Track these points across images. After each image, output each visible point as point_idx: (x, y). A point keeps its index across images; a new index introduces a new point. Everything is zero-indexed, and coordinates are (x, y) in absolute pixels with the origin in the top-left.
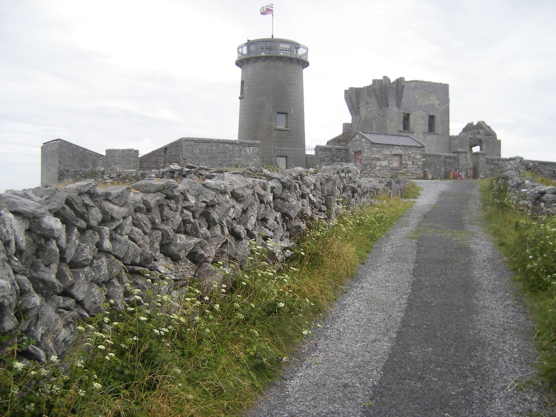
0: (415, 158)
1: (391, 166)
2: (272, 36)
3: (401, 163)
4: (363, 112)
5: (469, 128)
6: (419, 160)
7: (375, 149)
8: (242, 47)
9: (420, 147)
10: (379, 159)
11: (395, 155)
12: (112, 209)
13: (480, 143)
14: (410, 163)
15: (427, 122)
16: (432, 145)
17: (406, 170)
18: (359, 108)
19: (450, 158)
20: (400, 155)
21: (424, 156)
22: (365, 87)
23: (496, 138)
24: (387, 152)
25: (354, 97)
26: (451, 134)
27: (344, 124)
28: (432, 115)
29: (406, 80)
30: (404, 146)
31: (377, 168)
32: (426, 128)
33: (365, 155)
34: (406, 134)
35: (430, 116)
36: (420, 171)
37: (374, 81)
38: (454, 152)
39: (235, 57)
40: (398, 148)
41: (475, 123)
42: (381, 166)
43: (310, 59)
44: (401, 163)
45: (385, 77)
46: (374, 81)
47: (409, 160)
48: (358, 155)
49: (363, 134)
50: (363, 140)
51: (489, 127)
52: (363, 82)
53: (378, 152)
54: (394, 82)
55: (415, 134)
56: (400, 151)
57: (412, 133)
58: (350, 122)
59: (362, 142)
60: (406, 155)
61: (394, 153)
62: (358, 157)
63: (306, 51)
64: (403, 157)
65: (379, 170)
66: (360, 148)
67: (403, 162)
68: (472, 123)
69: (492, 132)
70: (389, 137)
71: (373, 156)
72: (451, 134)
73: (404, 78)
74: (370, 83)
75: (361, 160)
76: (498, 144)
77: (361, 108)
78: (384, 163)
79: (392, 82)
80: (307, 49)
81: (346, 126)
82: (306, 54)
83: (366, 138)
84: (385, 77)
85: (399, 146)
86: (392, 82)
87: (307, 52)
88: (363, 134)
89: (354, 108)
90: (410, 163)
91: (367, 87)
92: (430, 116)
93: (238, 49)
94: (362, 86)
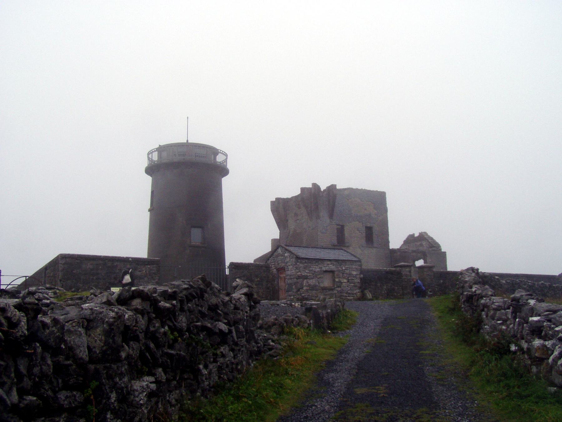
0: (350, 274)
1: (322, 285)
2: (187, 141)
3: (334, 281)
4: (292, 225)
5: (411, 240)
6: (355, 276)
7: (301, 265)
8: (152, 153)
9: (355, 261)
10: (306, 277)
11: (326, 271)
12: (312, 305)
13: (423, 256)
14: (345, 281)
15: (364, 234)
16: (372, 261)
17: (339, 289)
18: (287, 221)
19: (392, 274)
20: (332, 272)
21: (362, 272)
22: (292, 197)
23: (441, 250)
24: (316, 268)
25: (282, 209)
26: (391, 248)
27: (272, 240)
28: (369, 226)
29: (338, 187)
30: (337, 261)
31: (305, 288)
32: (363, 241)
33: (289, 273)
34: (339, 248)
35: (367, 227)
36: (358, 291)
37: (303, 189)
38: (395, 267)
39: (145, 164)
40: (329, 263)
41: (417, 235)
42: (309, 285)
43: (229, 166)
44: (334, 281)
45: (314, 185)
46: (303, 189)
47: (344, 278)
48: (281, 273)
49: (287, 248)
50: (286, 255)
51: (432, 239)
52: (291, 191)
53: (305, 268)
54: (324, 190)
55: (351, 248)
56: (332, 267)
57: (348, 247)
58: (278, 238)
59: (286, 257)
60: (339, 271)
61: (324, 269)
62: (282, 276)
63: (224, 157)
64: (336, 273)
65: (307, 290)
66: (283, 264)
67: (337, 280)
68: (414, 235)
69: (437, 243)
70: (319, 250)
71: (299, 273)
72: (391, 248)
73: (335, 185)
74: (298, 192)
75: (285, 279)
76: (443, 256)
77: (289, 221)
78: (312, 282)
79: (322, 190)
80: (226, 155)
81: (274, 241)
82: (226, 160)
83: (290, 252)
84: (314, 185)
85: (330, 260)
86: (322, 190)
87: (227, 158)
88: (287, 248)
89: (281, 222)
90: (345, 281)
91: (296, 196)
92: (367, 227)
93: (148, 154)
94: (290, 197)
